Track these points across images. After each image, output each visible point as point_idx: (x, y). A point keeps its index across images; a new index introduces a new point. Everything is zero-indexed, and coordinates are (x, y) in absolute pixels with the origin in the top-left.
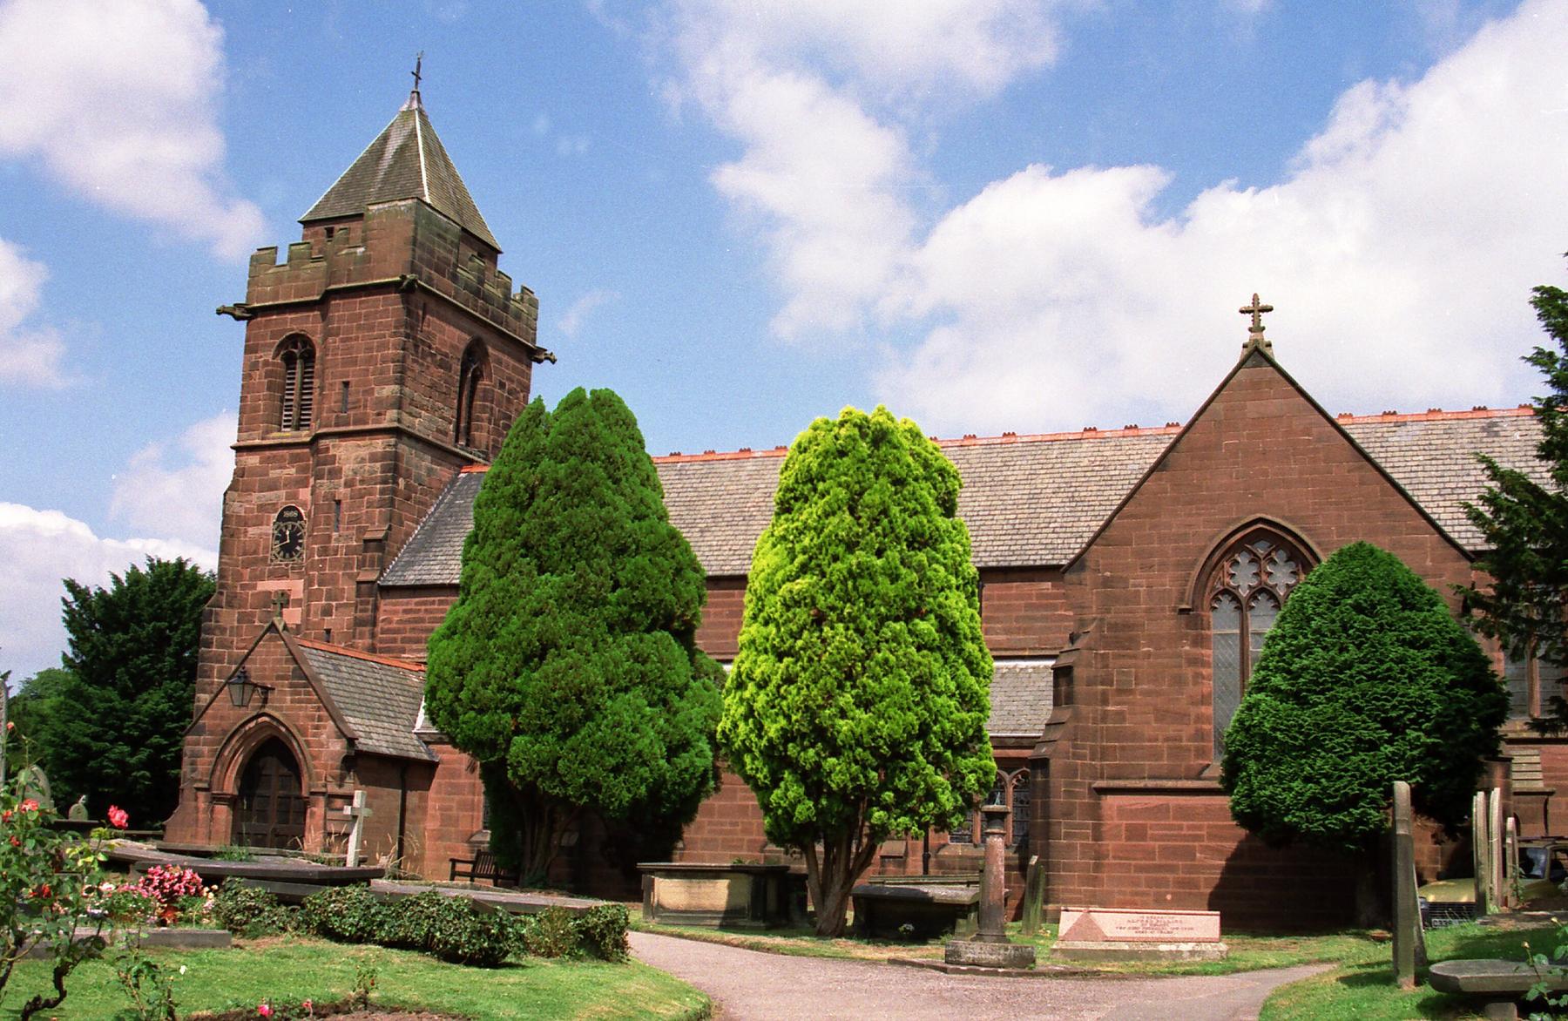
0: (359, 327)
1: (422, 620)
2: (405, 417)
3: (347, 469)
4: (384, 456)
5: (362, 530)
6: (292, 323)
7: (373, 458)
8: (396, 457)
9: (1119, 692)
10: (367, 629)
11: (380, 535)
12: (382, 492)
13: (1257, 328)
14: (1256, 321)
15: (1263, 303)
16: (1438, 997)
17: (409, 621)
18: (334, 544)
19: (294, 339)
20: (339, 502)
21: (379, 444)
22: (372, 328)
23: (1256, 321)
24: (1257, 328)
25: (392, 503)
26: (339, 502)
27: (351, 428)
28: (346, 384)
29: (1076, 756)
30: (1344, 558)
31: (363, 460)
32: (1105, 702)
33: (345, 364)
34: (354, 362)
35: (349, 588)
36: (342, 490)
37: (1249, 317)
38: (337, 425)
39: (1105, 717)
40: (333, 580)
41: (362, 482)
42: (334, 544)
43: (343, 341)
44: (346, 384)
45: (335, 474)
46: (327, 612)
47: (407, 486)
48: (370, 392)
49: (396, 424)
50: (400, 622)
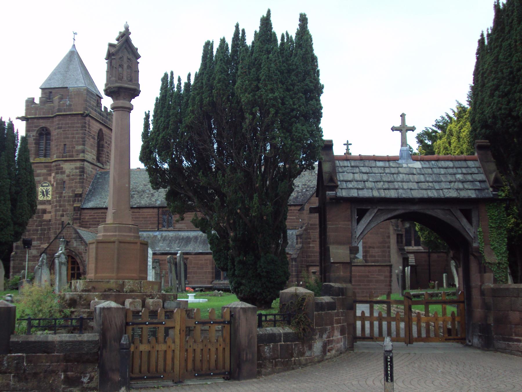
0: (69, 127)
1: (96, 218)
2: (86, 155)
3: (67, 172)
4: (80, 168)
5: (73, 191)
6: (43, 124)
7: (76, 168)
8: (83, 168)
9: (313, 241)
10: (78, 221)
11: (81, 192)
12: (80, 179)
13: (348, 149)
14: (348, 147)
15: (349, 143)
16: (4, 129)
17: (91, 219)
18: (64, 195)
19: (43, 129)
20: (64, 182)
21: (78, 164)
22: (73, 127)
23: (348, 147)
24: (348, 149)
25: (83, 182)
26: (64, 182)
27: (68, 159)
28: (65, 145)
29: (303, 257)
30: (384, 338)
31: (72, 169)
32: (309, 244)
33: (65, 138)
34: (68, 138)
35: (70, 208)
36: (66, 178)
37: (346, 146)
38: (63, 157)
39: (310, 247)
40: (64, 206)
41: (73, 175)
42: (64, 195)
43: (63, 131)
44: (65, 145)
45: (63, 173)
46: (62, 216)
47: (87, 177)
48: (74, 147)
49: (83, 158)
50: (88, 219)
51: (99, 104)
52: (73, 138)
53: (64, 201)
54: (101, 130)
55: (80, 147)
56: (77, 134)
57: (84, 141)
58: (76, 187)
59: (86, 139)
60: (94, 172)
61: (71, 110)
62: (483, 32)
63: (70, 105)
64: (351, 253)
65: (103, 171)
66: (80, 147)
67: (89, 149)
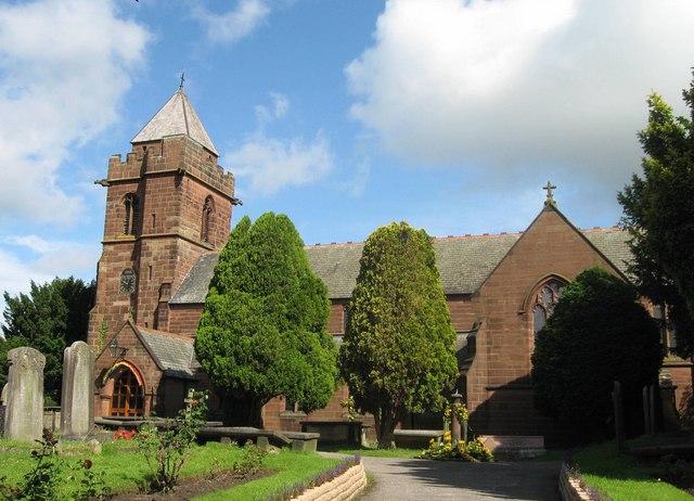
3: (155, 253)
4: (171, 247)
7: (166, 248)
9: (496, 347)
21: (169, 242)
51: (483, 456)
52: (165, 205)
53: (149, 294)
54: (210, 197)
55: (172, 218)
56: (169, 199)
57: (178, 210)
58: (165, 274)
59: (182, 206)
60: (197, 255)
61: (161, 168)
62: (635, 176)
63: (163, 161)
64: (465, 377)
65: (210, 253)
66: (172, 218)
67: (186, 221)
